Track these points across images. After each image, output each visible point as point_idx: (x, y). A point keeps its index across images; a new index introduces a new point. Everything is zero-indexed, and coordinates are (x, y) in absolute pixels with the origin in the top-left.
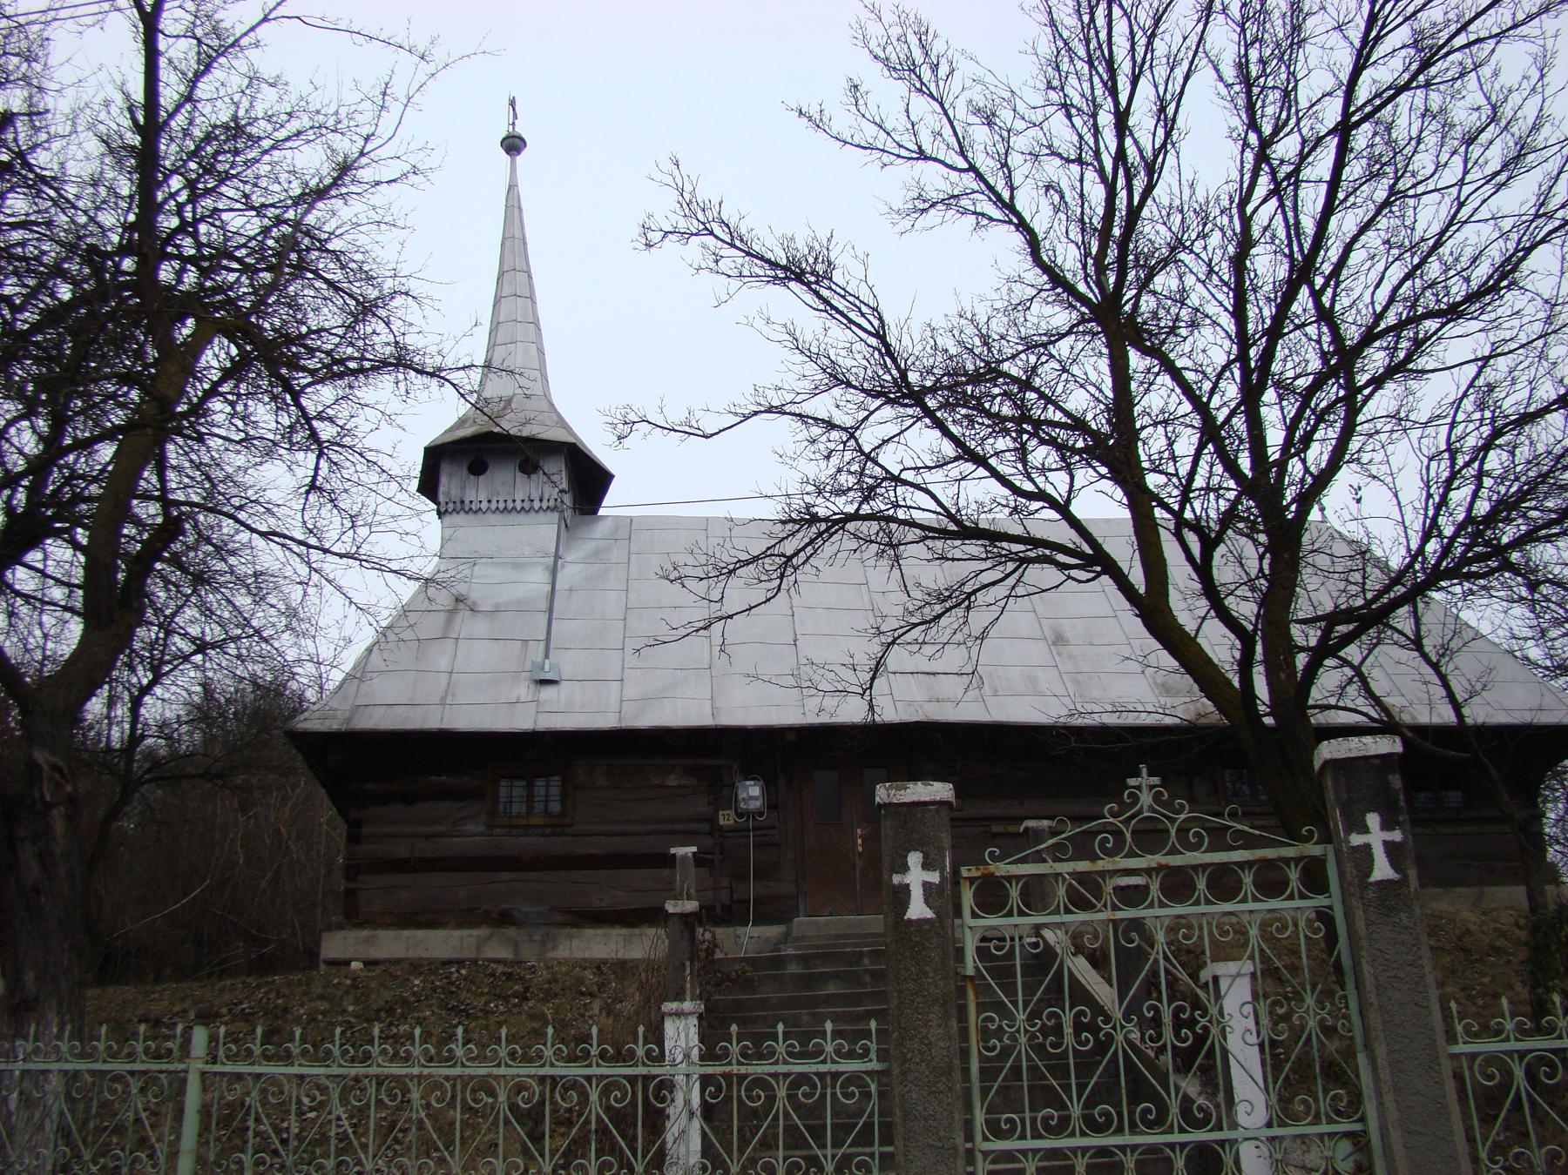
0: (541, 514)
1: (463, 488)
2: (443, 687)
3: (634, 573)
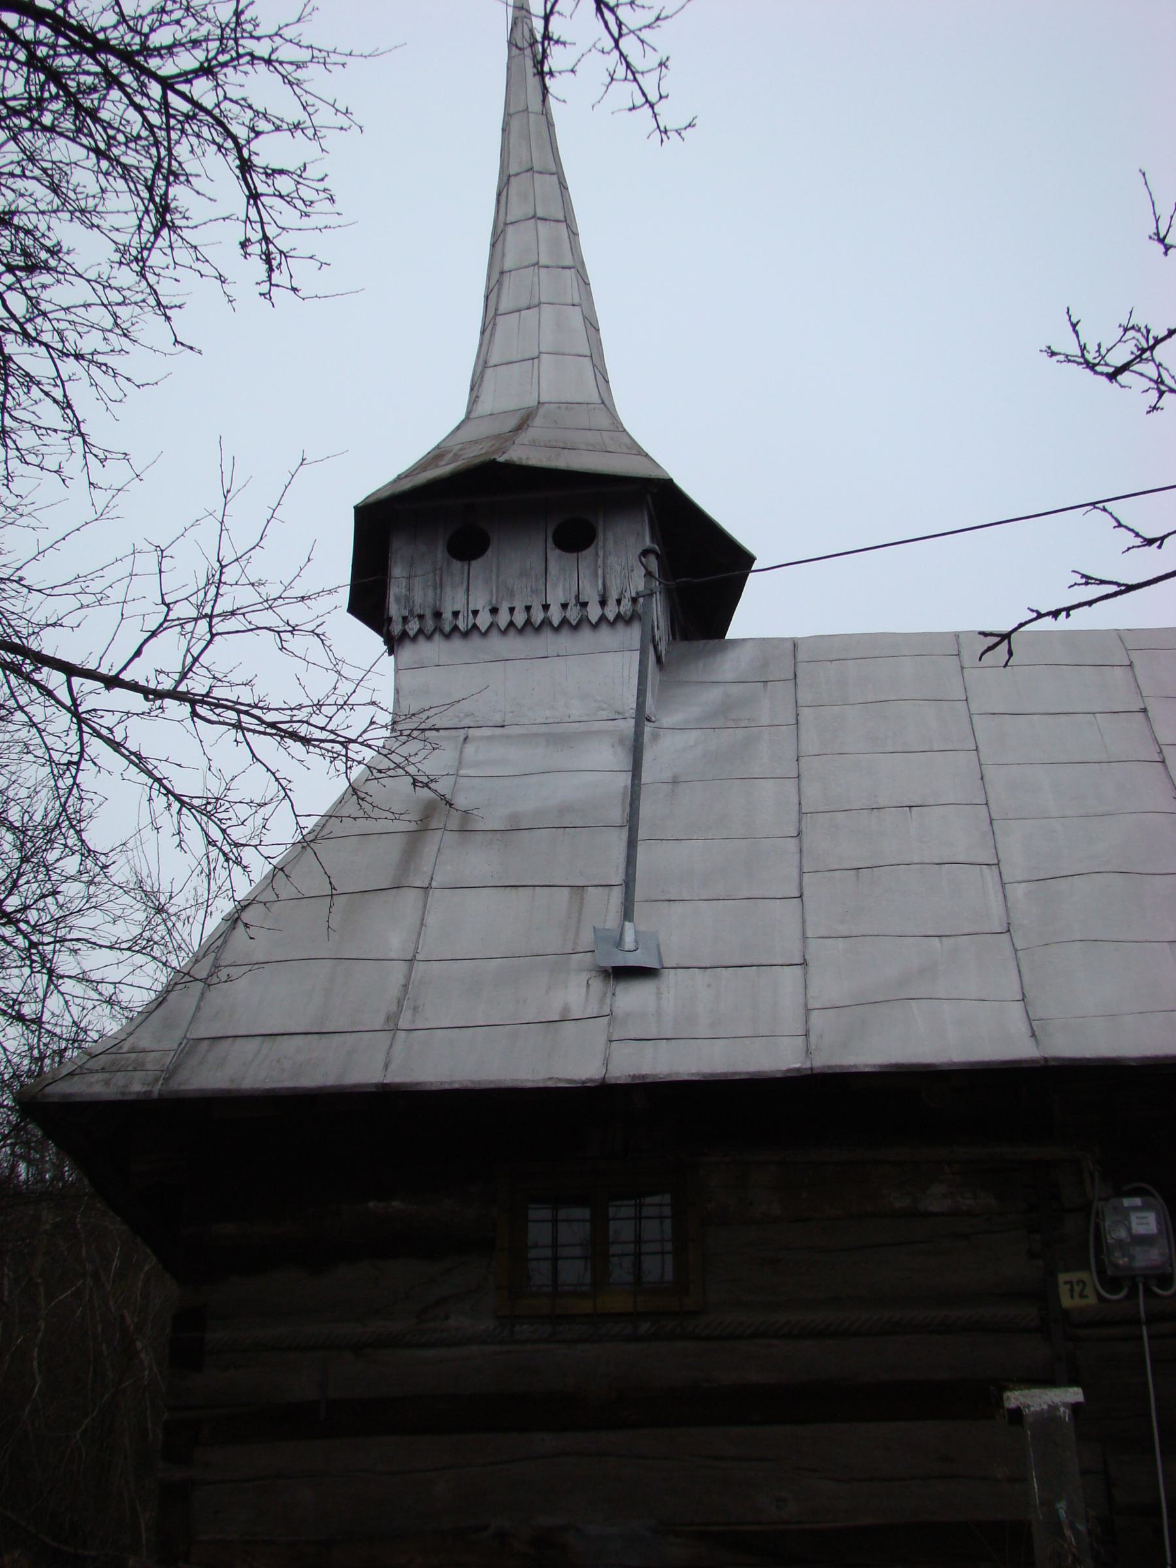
0: (604, 630)
1: (439, 586)
2: (394, 991)
3: (811, 741)
